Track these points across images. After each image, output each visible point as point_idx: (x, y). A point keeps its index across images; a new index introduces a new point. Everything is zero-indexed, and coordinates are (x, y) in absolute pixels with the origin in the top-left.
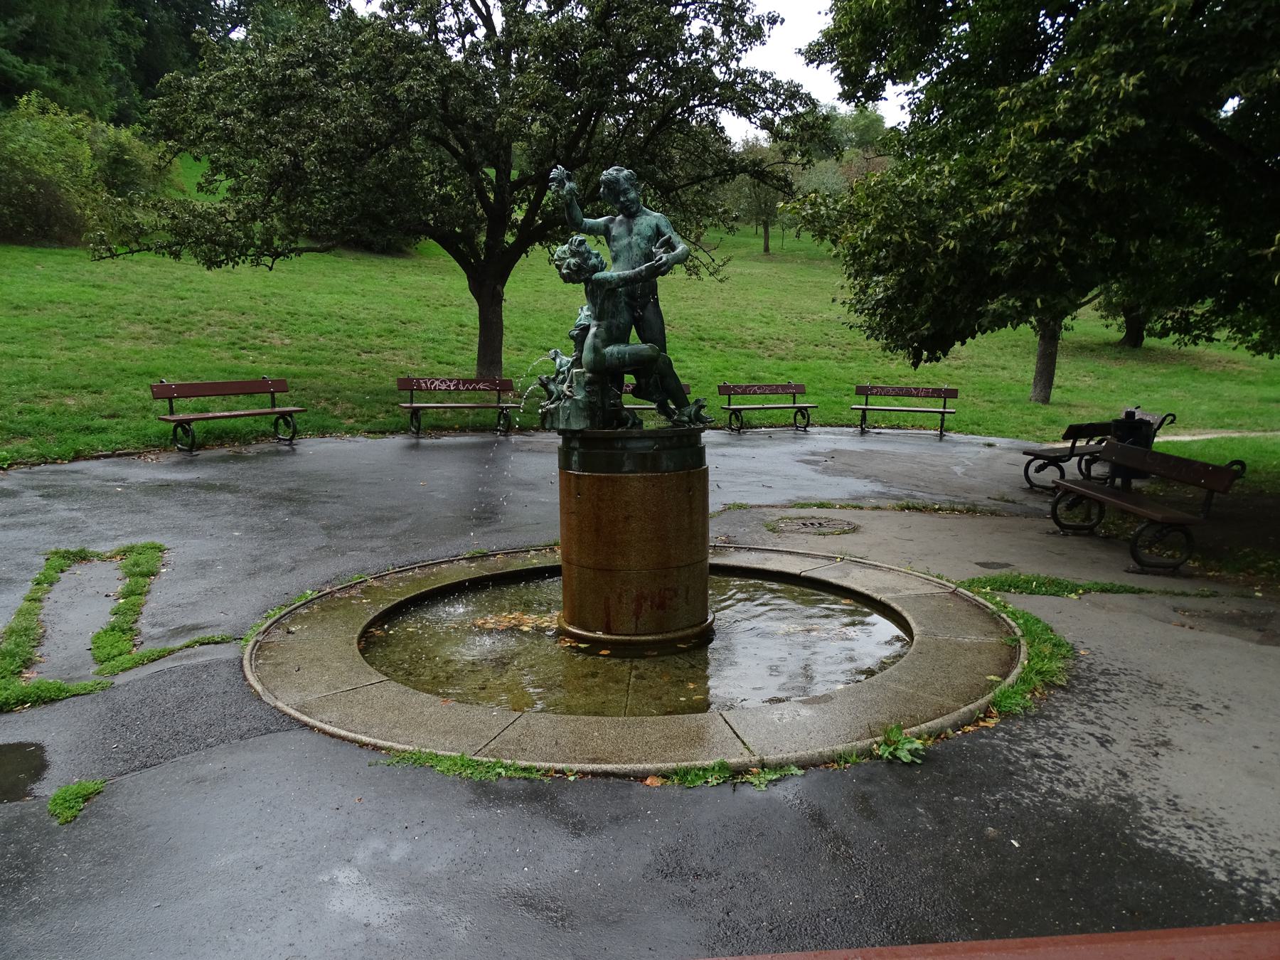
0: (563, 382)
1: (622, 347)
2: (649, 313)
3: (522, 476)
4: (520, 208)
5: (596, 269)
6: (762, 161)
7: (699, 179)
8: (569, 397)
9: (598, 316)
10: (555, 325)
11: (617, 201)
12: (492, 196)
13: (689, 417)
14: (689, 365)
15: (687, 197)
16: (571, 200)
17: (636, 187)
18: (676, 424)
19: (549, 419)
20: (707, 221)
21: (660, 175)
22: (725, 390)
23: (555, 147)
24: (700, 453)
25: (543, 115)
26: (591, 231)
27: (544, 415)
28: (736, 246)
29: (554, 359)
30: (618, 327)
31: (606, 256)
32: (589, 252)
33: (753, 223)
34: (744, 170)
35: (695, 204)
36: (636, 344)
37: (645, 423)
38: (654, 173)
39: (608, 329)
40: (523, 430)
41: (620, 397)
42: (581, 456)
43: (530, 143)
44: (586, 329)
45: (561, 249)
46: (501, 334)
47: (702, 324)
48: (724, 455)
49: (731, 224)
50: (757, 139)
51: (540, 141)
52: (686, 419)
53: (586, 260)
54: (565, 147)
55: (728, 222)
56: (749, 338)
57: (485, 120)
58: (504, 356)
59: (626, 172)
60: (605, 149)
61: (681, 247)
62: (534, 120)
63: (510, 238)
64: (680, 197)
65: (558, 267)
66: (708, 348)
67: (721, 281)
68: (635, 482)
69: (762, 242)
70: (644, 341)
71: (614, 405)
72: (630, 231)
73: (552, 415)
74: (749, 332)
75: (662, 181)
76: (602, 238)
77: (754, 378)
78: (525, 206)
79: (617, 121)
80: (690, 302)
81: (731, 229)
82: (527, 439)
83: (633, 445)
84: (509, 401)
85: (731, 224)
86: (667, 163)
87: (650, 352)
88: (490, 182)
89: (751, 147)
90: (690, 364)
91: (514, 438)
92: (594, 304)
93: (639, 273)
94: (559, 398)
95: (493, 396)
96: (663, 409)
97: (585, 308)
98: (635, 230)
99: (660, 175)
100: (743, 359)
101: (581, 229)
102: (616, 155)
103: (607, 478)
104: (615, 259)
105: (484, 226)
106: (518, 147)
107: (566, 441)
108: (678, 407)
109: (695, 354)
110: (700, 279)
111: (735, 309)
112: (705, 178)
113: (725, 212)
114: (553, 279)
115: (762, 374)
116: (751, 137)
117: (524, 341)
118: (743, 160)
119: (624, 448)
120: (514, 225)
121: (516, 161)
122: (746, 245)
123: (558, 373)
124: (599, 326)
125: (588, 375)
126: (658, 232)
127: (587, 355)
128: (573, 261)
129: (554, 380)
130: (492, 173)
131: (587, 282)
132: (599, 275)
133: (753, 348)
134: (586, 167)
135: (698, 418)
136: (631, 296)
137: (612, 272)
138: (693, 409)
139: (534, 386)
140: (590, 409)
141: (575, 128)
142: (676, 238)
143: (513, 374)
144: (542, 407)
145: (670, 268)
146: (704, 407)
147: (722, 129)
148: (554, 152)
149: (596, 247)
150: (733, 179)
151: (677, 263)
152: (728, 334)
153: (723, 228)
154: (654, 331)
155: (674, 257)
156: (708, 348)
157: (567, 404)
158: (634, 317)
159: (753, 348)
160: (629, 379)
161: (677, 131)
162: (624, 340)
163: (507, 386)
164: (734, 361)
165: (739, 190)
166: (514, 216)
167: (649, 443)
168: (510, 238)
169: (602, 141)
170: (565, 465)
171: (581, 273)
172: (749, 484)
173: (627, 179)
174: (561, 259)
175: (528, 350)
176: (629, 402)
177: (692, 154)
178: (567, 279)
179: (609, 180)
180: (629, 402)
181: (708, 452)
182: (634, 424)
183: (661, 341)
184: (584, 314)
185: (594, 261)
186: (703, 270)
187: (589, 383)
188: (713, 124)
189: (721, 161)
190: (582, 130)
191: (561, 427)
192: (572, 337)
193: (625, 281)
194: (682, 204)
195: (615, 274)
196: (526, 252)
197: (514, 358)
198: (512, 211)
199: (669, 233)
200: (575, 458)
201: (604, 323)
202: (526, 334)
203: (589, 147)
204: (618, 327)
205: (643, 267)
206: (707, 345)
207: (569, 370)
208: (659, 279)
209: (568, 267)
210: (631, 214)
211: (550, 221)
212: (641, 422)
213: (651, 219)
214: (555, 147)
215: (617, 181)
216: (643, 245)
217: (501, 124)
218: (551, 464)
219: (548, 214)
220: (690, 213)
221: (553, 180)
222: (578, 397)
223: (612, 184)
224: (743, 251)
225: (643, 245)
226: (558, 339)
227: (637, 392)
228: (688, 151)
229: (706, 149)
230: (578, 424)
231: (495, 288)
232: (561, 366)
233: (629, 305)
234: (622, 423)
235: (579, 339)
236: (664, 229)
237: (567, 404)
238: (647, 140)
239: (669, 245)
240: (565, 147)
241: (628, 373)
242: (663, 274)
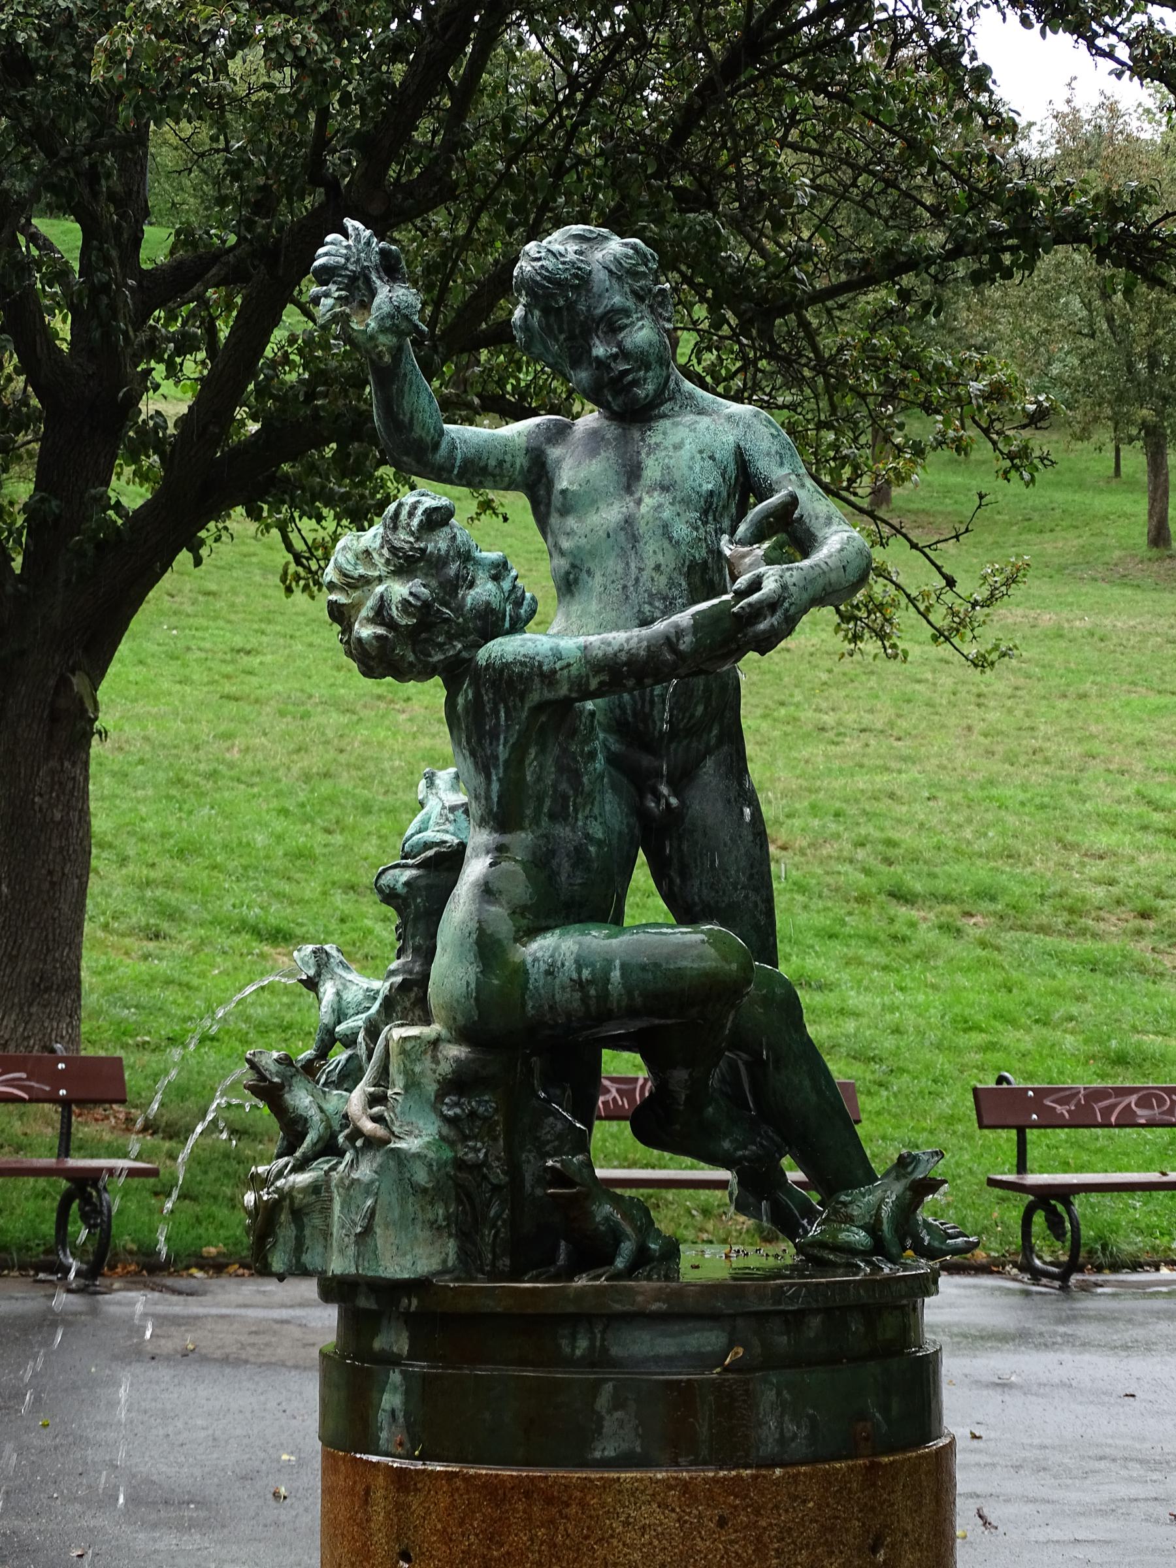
0: (348, 1077)
1: (595, 940)
2: (706, 801)
3: (162, 1467)
4: (173, 371)
5: (491, 623)
6: (1142, 196)
7: (891, 265)
8: (373, 1143)
9: (502, 816)
10: (300, 836)
11: (579, 355)
12: (62, 326)
13: (873, 1229)
14: (864, 1004)
15: (839, 334)
16: (398, 352)
17: (655, 303)
18: (815, 1257)
19: (286, 1231)
20: (921, 427)
21: (738, 253)
22: (1005, 1108)
23: (321, 143)
24: (918, 1383)
25: (276, 25)
26: (475, 472)
27: (266, 1220)
28: (1029, 523)
29: (312, 984)
30: (579, 856)
31: (536, 577)
32: (466, 557)
33: (1104, 435)
34: (1071, 232)
35: (875, 360)
36: (648, 926)
37: (688, 1255)
38: (710, 242)
39: (540, 864)
40: (151, 1269)
41: (581, 1143)
42: (422, 1392)
43: (223, 127)
44: (445, 863)
45: (357, 545)
46: (83, 870)
47: (905, 836)
48: (1003, 1385)
49: (1017, 438)
50: (1114, 112)
51: (262, 117)
52: (859, 1237)
53: (452, 587)
54: (361, 142)
55: (1008, 429)
56: (1099, 893)
57: (47, 39)
58: (90, 960)
59: (615, 246)
60: (517, 150)
61: (837, 538)
62: (240, 40)
63: (129, 491)
64: (811, 335)
65: (340, 615)
66: (926, 935)
67: (980, 663)
68: (642, 1501)
69: (1139, 506)
70: (685, 913)
71: (559, 1178)
72: (631, 475)
73: (298, 1215)
74: (1096, 869)
75: (745, 272)
76: (516, 503)
77: (1121, 1060)
78: (192, 366)
79: (566, 48)
80: (852, 746)
81: (1018, 461)
82: (176, 1306)
83: (641, 1344)
84: (112, 1152)
85: (1017, 438)
86: (766, 204)
87: (711, 959)
88: (60, 274)
89: (1090, 143)
90: (854, 1000)
91: (133, 1303)
92: (484, 765)
93: (670, 641)
94: (329, 1148)
95: (41, 1124)
96: (758, 1189)
97: (444, 777)
98: (652, 470)
99: (738, 253)
100: (1072, 980)
101: (423, 459)
102: (559, 172)
103: (528, 1489)
104: (568, 584)
105: (28, 441)
106: (168, 142)
107: (357, 1325)
108: (820, 1178)
109: (874, 955)
110: (895, 654)
111: (1037, 775)
112: (915, 262)
113: (997, 393)
114: (304, 651)
115: (1153, 1042)
116: (1087, 102)
117: (174, 897)
118: (1064, 194)
119: (599, 1360)
120: (150, 438)
121: (158, 192)
122: (1077, 519)
123: (328, 1040)
124: (500, 850)
125: (455, 1051)
126: (745, 481)
127: (450, 972)
128: (399, 590)
129: (309, 1069)
130: (64, 234)
131: (455, 674)
132: (504, 648)
133: (1114, 938)
134: (438, 218)
135: (903, 1232)
136: (632, 730)
137: (560, 636)
138: (885, 1196)
139: (229, 1097)
140: (459, 1195)
141: (398, 71)
142: (815, 505)
143: (123, 1032)
144: (258, 1182)
145: (789, 625)
146: (932, 1185)
147: (981, 77)
148: (316, 163)
149: (502, 537)
150: (1029, 265)
151: (818, 601)
152: (1007, 876)
153: (983, 450)
154: (727, 880)
155: (808, 581)
156: (926, 935)
157: (365, 1171)
158: (640, 813)
159: (1114, 938)
160: (623, 1066)
161: (802, 84)
162: (604, 908)
163: (96, 1086)
164: (1036, 985)
165: (1045, 305)
166: (149, 405)
167: (708, 1339)
168: (129, 491)
169: (507, 121)
170: (348, 1427)
171: (432, 637)
172: (1108, 1510)
173: (620, 272)
174: (352, 583)
175: (190, 935)
176: (617, 1155)
177: (858, 170)
178: (375, 661)
179: (551, 278)
180: (617, 1155)
181: (953, 1368)
182: (641, 1259)
183: (750, 911)
184: (441, 801)
185: (483, 591)
186: (905, 617)
187: (458, 1084)
188: (946, 57)
189: (978, 199)
190: (427, 77)
191: (338, 1265)
192: (389, 896)
193: (613, 673)
194: (821, 364)
195: (570, 644)
196: (195, 547)
197: (130, 968)
198: (144, 383)
199: (788, 479)
200: (391, 1400)
201: (521, 841)
202: (183, 871)
203: (455, 141)
204: (579, 856)
205: (684, 618)
206: (924, 922)
207: (373, 1031)
208: (751, 670)
209: (380, 615)
210: (634, 407)
211: (291, 431)
212: (672, 1250)
213: (710, 429)
214: (321, 143)
215: (581, 280)
216: (681, 530)
217: (114, 56)
218: (289, 1416)
219: (286, 397)
220: (863, 406)
221: (326, 275)
222: (410, 1144)
223: (562, 295)
224: (1062, 544)
225: (681, 530)
226: (311, 889)
227: (654, 1124)
228: (847, 160)
229: (917, 151)
230: (410, 1255)
231: (64, 683)
232: (340, 1015)
233: (627, 765)
234: (593, 1252)
235: (419, 901)
236: (769, 467)
237: (365, 1171)
238: (686, 121)
239: (790, 533)
240: (361, 142)
241: (619, 1044)
242: (764, 644)
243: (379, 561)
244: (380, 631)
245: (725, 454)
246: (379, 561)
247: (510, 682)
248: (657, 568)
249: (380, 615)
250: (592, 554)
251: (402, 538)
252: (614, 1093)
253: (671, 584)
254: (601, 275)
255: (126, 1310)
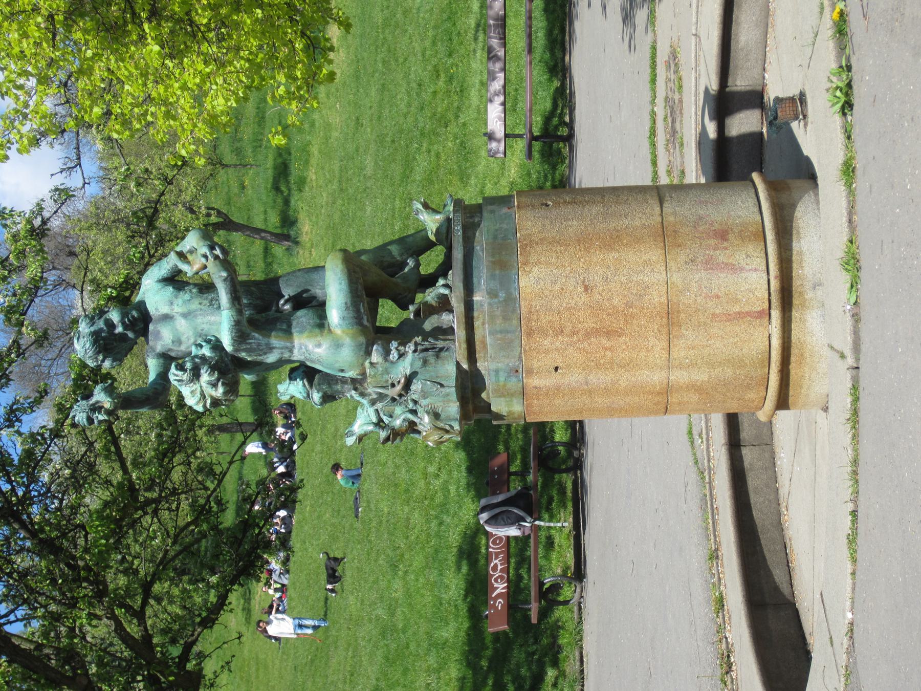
209: (214, 385)
243: (195, 387)
244: (220, 384)
245: (159, 285)
246: (194, 388)
247: (239, 337)
248: (200, 304)
249: (214, 385)
250: (195, 329)
251: (185, 377)
252: (497, 561)
253: (207, 299)
254: (92, 329)
255: (483, 502)
